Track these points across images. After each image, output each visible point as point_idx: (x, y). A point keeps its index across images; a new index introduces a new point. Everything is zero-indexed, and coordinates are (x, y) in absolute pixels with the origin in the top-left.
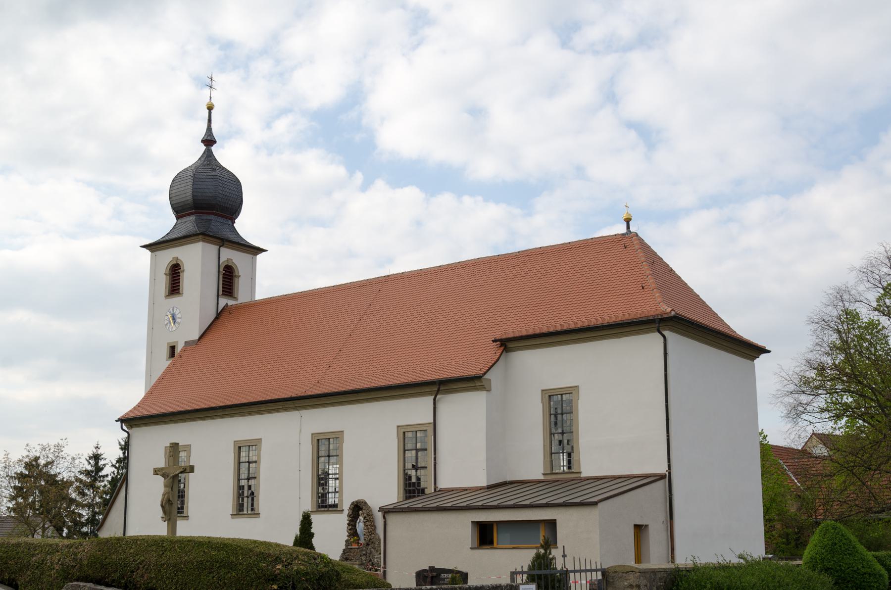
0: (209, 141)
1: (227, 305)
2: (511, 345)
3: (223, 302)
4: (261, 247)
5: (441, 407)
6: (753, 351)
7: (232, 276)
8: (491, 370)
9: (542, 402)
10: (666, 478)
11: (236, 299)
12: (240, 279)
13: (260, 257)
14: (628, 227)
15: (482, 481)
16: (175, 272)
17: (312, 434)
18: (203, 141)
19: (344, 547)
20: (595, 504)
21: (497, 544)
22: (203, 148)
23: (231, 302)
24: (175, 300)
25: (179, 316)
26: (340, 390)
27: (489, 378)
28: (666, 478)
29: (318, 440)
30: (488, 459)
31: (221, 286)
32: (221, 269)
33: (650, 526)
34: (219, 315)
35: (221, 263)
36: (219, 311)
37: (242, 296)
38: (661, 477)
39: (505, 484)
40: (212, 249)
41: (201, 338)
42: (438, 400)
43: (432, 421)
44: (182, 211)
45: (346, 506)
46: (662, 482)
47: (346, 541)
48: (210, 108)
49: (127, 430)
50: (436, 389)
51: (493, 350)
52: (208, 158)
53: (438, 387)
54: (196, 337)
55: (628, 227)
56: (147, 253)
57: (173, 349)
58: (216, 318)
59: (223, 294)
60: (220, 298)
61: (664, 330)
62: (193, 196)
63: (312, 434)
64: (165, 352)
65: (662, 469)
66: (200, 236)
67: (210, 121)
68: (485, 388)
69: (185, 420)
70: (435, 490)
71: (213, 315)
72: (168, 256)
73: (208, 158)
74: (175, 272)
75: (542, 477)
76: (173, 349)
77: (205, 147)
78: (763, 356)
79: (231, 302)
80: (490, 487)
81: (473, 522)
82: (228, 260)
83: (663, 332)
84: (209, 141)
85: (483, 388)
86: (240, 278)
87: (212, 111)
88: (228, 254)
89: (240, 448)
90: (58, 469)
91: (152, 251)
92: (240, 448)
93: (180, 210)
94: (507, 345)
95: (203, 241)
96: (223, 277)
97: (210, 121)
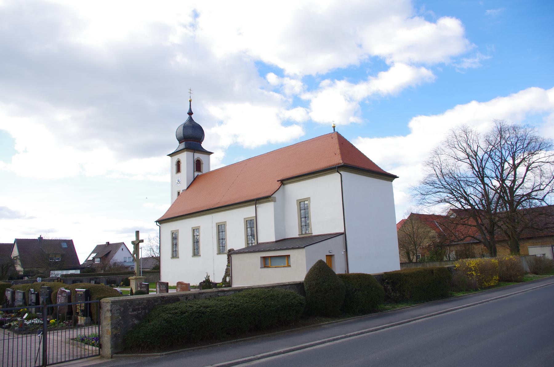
0: (190, 113)
1: (198, 175)
2: (284, 182)
3: (196, 174)
4: (212, 152)
5: (258, 209)
6: (392, 177)
7: (200, 164)
8: (275, 193)
9: (297, 205)
10: (344, 234)
11: (202, 172)
12: (181, 164)
13: (211, 156)
14: (334, 130)
15: (274, 240)
16: (178, 163)
17: (216, 223)
18: (188, 113)
19: (226, 268)
20: (304, 247)
21: (271, 266)
22: (188, 116)
23: (200, 174)
24: (179, 174)
25: (180, 181)
26: (225, 205)
27: (275, 196)
28: (344, 234)
29: (219, 226)
30: (275, 230)
31: (195, 166)
32: (195, 161)
33: (335, 256)
34: (195, 179)
35: (194, 159)
36: (195, 178)
37: (204, 170)
38: (342, 234)
39: (285, 239)
40: (191, 154)
41: (187, 188)
42: (257, 207)
43: (255, 216)
44: (181, 140)
45: (226, 251)
46: (342, 235)
47: (227, 265)
48: (190, 101)
49: (160, 225)
50: (255, 203)
51: (279, 184)
52: (191, 119)
53: (255, 201)
54: (186, 188)
55: (334, 130)
56: (169, 157)
57: (179, 193)
58: (194, 180)
59: (196, 171)
60: (195, 173)
61: (341, 171)
62: (183, 134)
63: (216, 223)
64: (176, 194)
65: (342, 231)
66: (185, 149)
67: (190, 106)
68: (274, 200)
69: (199, 216)
70: (257, 244)
71: (193, 179)
72: (176, 158)
73: (191, 119)
74: (178, 163)
75: (298, 236)
76: (179, 193)
77: (189, 116)
78: (396, 179)
79: (200, 174)
80: (276, 242)
81: (261, 257)
82: (198, 158)
83: (340, 172)
84: (190, 113)
85: (272, 201)
86: (203, 164)
87: (191, 102)
88: (198, 156)
89: (194, 230)
90: (252, 242)
91: (171, 157)
92: (194, 230)
93: (180, 141)
94: (283, 182)
95: (187, 151)
96: (196, 164)
97: (190, 106)
